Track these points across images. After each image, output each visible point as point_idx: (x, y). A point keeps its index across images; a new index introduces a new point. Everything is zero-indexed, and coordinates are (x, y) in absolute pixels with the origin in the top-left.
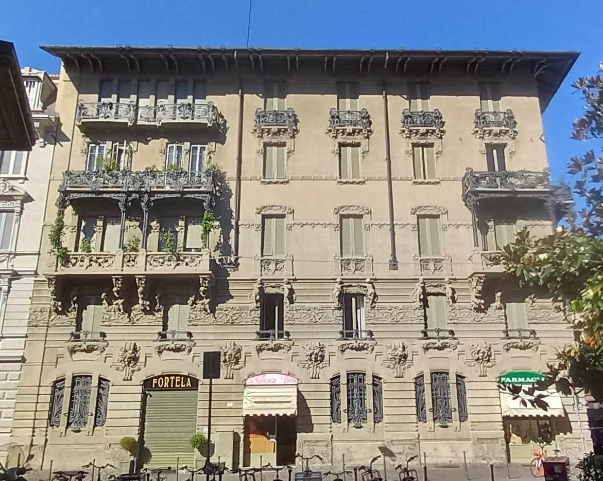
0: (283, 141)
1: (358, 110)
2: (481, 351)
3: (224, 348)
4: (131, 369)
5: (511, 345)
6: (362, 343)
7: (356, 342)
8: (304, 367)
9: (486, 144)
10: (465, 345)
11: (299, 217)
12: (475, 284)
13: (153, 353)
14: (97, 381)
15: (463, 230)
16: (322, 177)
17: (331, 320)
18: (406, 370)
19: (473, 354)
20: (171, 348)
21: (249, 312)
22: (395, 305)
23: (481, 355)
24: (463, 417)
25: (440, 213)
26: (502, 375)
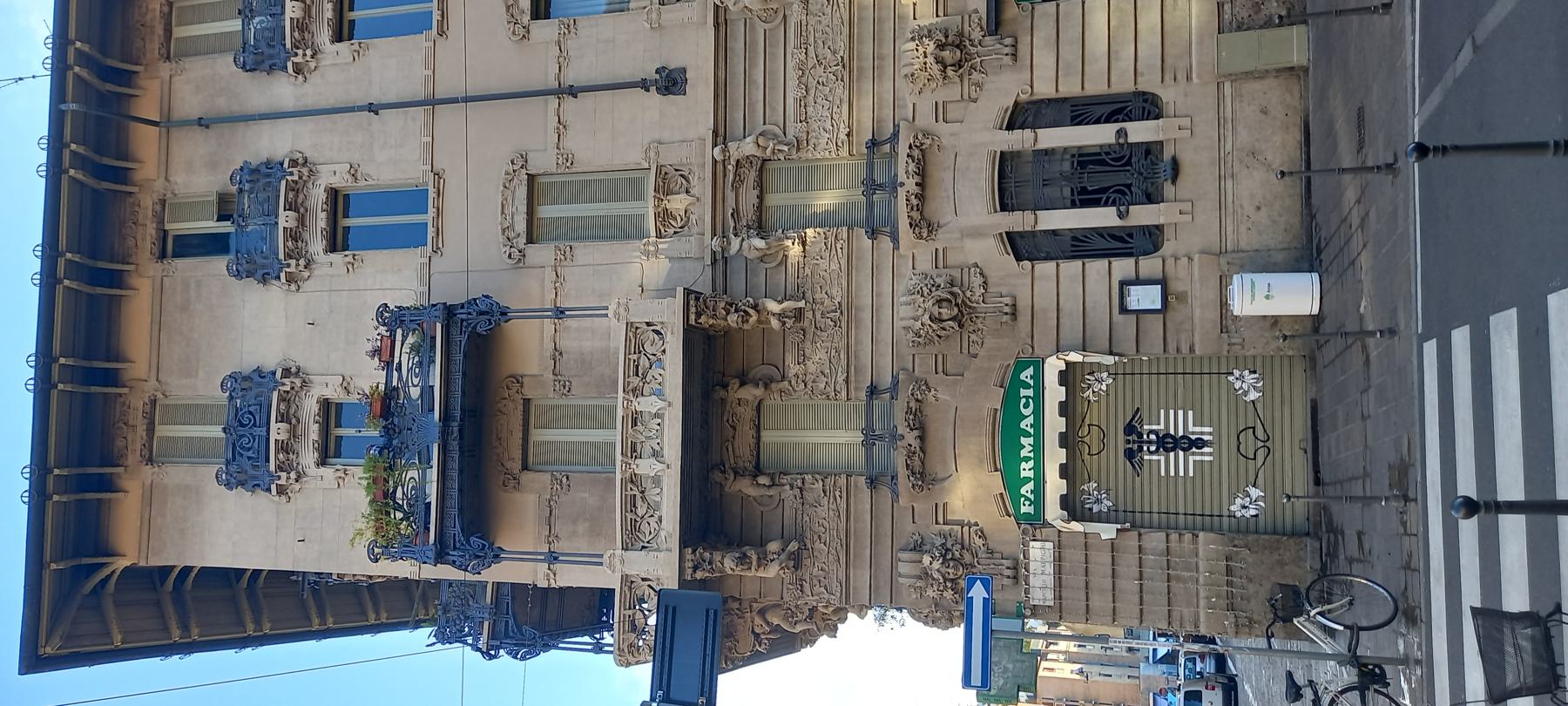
0: (323, 196)
2: (936, 310)
5: (916, 215)
7: (902, 184)
9: (322, 462)
10: (920, 105)
13: (932, 246)
17: (837, 21)
20: (917, 190)
21: (812, 20)
22: (793, 75)
24: (1146, 106)
26: (1011, 511)
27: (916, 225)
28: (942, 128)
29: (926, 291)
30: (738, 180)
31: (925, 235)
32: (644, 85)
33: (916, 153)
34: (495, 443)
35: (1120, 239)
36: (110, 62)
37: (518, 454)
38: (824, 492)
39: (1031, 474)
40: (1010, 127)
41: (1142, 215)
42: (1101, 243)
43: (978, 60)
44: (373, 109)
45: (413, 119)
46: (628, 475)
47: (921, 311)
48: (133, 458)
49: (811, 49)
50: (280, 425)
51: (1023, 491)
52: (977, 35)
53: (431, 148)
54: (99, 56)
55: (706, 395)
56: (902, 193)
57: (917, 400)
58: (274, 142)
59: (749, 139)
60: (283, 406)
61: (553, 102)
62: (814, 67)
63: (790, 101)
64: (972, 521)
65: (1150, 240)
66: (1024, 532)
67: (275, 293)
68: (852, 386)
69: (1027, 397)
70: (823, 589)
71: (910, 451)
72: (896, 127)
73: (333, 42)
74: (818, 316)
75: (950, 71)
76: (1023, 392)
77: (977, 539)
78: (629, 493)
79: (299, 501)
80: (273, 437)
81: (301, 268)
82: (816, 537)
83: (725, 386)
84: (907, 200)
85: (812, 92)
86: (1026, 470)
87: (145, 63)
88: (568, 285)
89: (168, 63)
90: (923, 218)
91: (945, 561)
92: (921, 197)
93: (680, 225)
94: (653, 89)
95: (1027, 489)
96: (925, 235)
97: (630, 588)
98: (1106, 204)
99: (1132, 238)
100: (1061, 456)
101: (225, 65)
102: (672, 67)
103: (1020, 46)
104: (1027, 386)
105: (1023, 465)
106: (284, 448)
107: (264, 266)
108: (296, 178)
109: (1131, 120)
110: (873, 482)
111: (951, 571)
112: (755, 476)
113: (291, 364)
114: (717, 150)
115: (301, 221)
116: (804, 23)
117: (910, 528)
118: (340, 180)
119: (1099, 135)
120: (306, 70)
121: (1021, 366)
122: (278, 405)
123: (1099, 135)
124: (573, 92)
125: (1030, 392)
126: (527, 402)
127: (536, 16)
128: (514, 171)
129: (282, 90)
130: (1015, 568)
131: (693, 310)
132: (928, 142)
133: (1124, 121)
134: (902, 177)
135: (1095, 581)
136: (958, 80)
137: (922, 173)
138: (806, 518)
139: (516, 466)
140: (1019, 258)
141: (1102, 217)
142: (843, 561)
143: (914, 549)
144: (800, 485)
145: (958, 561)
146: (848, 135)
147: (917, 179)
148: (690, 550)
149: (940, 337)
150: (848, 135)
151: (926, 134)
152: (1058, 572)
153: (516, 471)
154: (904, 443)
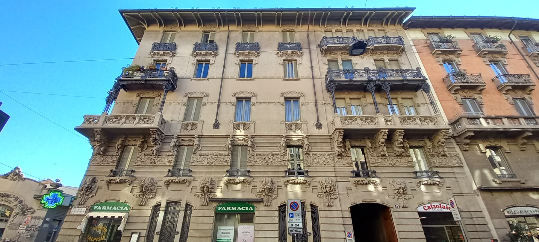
1: (295, 43)
2: (328, 186)
3: (143, 182)
4: (86, 197)
6: (182, 178)
7: (366, 179)
8: (394, 198)
11: (260, 99)
12: (337, 137)
14: (185, 206)
15: (309, 105)
16: (267, 77)
18: (273, 200)
19: (323, 188)
23: (328, 189)
25: (300, 96)
27: (287, 182)
28: (190, 187)
29: (333, 184)
30: (190, 140)
31: (165, 183)
33: (185, 181)
34: (339, 92)
35: (283, 233)
36: (369, 20)
37: (144, 96)
38: (227, 160)
39: (227, 210)
42: (283, 228)
43: (204, 196)
46: (122, 117)
47: (327, 183)
48: (283, 28)
49: (216, 156)
50: (163, 52)
51: (224, 207)
52: (211, 196)
54: (348, 18)
55: (366, 135)
57: (127, 182)
58: (222, 50)
59: (308, 143)
60: (295, 53)
61: (217, 102)
62: (268, 158)
64: (279, 195)
66: (89, 207)
67: (191, 51)
68: (136, 167)
69: (246, 209)
70: (215, 160)
71: (363, 181)
72: (193, 176)
74: (154, 159)
75: (397, 191)
76: (247, 208)
77: (91, 195)
78: (118, 117)
80: (203, 51)
81: (280, 55)
82: (330, 159)
83: (368, 139)
85: (207, 157)
87: (243, 27)
88: (177, 105)
89: (281, 31)
90: (170, 183)
91: (269, 189)
92: (174, 182)
93: (237, 128)
96: (165, 183)
97: (153, 118)
99: (284, 236)
100: (102, 216)
101: (281, 40)
102: (220, 126)
103: (205, 207)
104: (248, 209)
105: (230, 208)
107: (280, 49)
108: (298, 53)
109: (313, 237)
111: (267, 190)
112: (231, 145)
113: (303, 54)
114: (197, 136)
116: (279, 155)
117: (276, 180)
118: (298, 62)
120: (235, 55)
122: (295, 52)
124: (219, 105)
126: (154, 98)
127: (285, 98)
128: (300, 94)
130: (81, 205)
131: (153, 130)
132: (308, 185)
133: (313, 235)
134: (179, 178)
135: (72, 224)
136: (395, 193)
137: (180, 183)
138: (109, 156)
140: (279, 207)
142: (97, 164)
143: (272, 182)
144: (117, 155)
145: (269, 192)
146: (194, 165)
147: (299, 182)
148: (388, 131)
149: (321, 188)
150: (194, 165)
151: (309, 184)
152: (77, 215)
153: (284, 96)
154: (365, 180)
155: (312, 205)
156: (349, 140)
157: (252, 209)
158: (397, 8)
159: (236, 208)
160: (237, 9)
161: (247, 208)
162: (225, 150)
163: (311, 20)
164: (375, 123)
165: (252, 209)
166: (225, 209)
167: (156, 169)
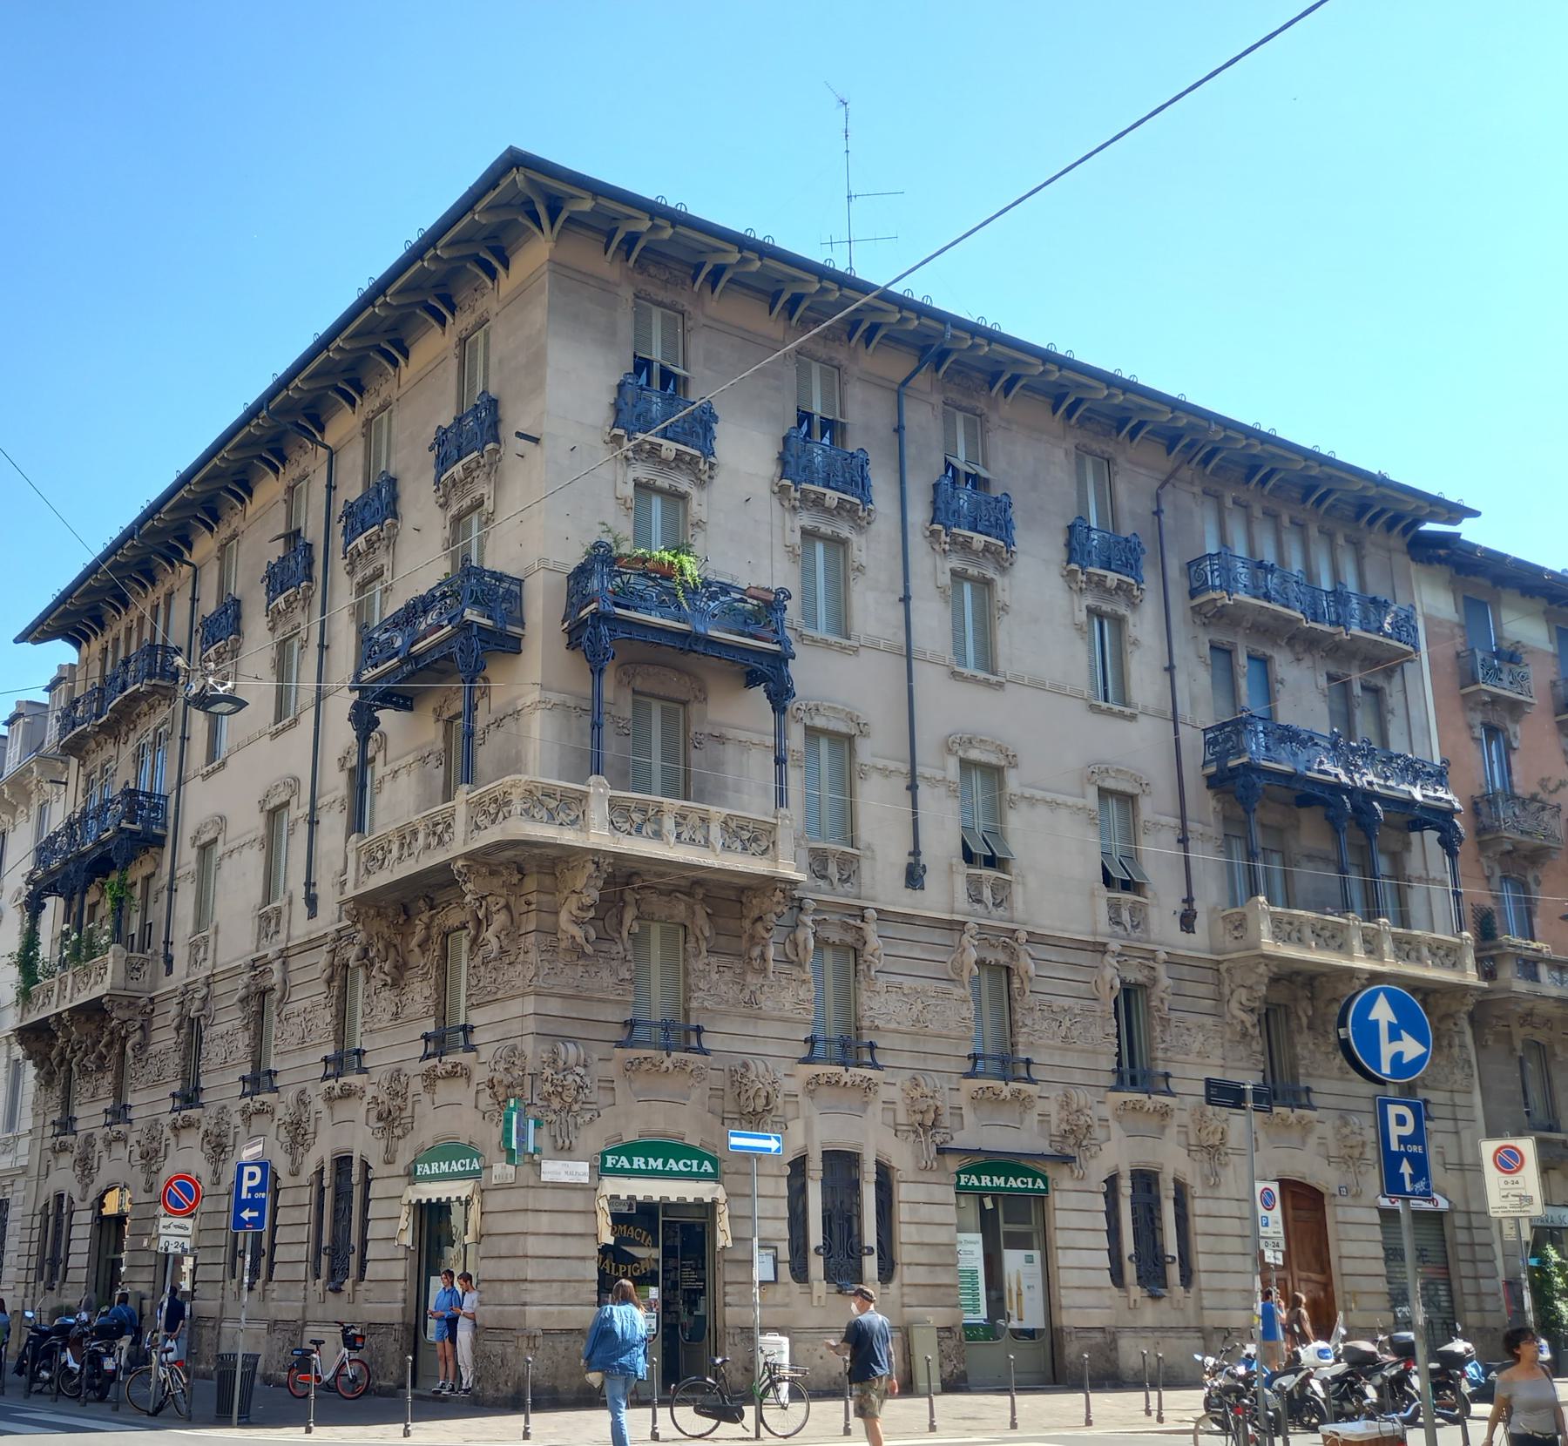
32: (916, 852)
39: (635, 1166)
40: (878, 1162)
41: (816, 1266)
44: (906, 599)
45: (895, 634)
51: (623, 1158)
53: (1037, 685)
56: (841, 1069)
63: (900, 979)
65: (800, 1272)
73: (1087, 607)
75: (919, 1117)
76: (695, 1163)
79: (604, 453)
84: (646, 1058)
86: (639, 1162)
94: (912, 860)
95: (624, 1162)
98: (824, 1238)
104: (699, 1167)
105: (642, 1160)
106: (655, 450)
108: (860, 514)
110: (630, 1025)
115: (664, 462)
119: (870, 1237)
121: (714, 1162)
123: (870, 1237)
124: (913, 788)
125: (695, 1169)
129: (919, 514)
139: (638, 683)
141: (816, 1237)
155: (1176, 1181)
156: (709, 911)
157: (1042, 1187)
158: (1177, 399)
159: (1002, 1179)
160: (990, 330)
161: (695, 1163)
162: (954, 976)
163: (1206, 461)
164: (572, 818)
165: (1042, 1187)
166: (977, 1184)
167: (764, 1029)
